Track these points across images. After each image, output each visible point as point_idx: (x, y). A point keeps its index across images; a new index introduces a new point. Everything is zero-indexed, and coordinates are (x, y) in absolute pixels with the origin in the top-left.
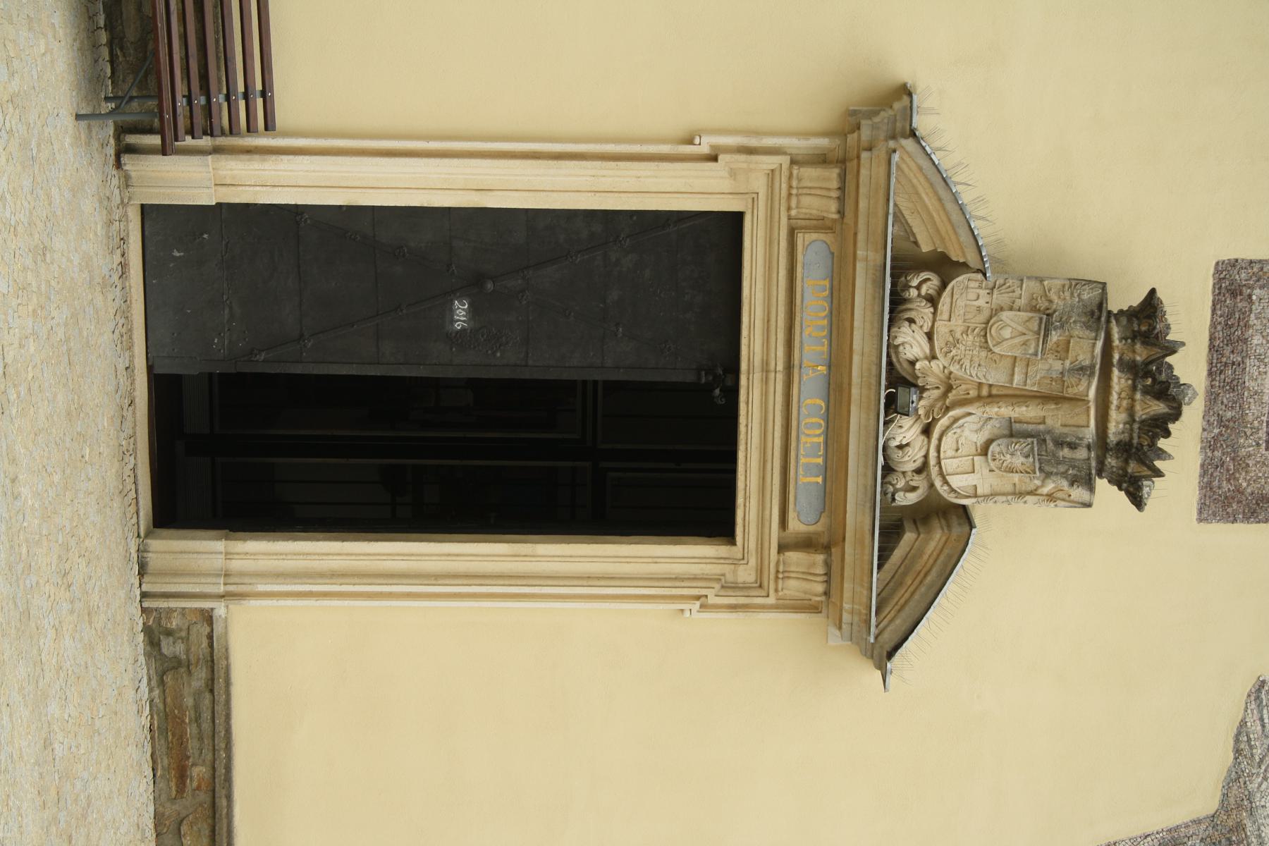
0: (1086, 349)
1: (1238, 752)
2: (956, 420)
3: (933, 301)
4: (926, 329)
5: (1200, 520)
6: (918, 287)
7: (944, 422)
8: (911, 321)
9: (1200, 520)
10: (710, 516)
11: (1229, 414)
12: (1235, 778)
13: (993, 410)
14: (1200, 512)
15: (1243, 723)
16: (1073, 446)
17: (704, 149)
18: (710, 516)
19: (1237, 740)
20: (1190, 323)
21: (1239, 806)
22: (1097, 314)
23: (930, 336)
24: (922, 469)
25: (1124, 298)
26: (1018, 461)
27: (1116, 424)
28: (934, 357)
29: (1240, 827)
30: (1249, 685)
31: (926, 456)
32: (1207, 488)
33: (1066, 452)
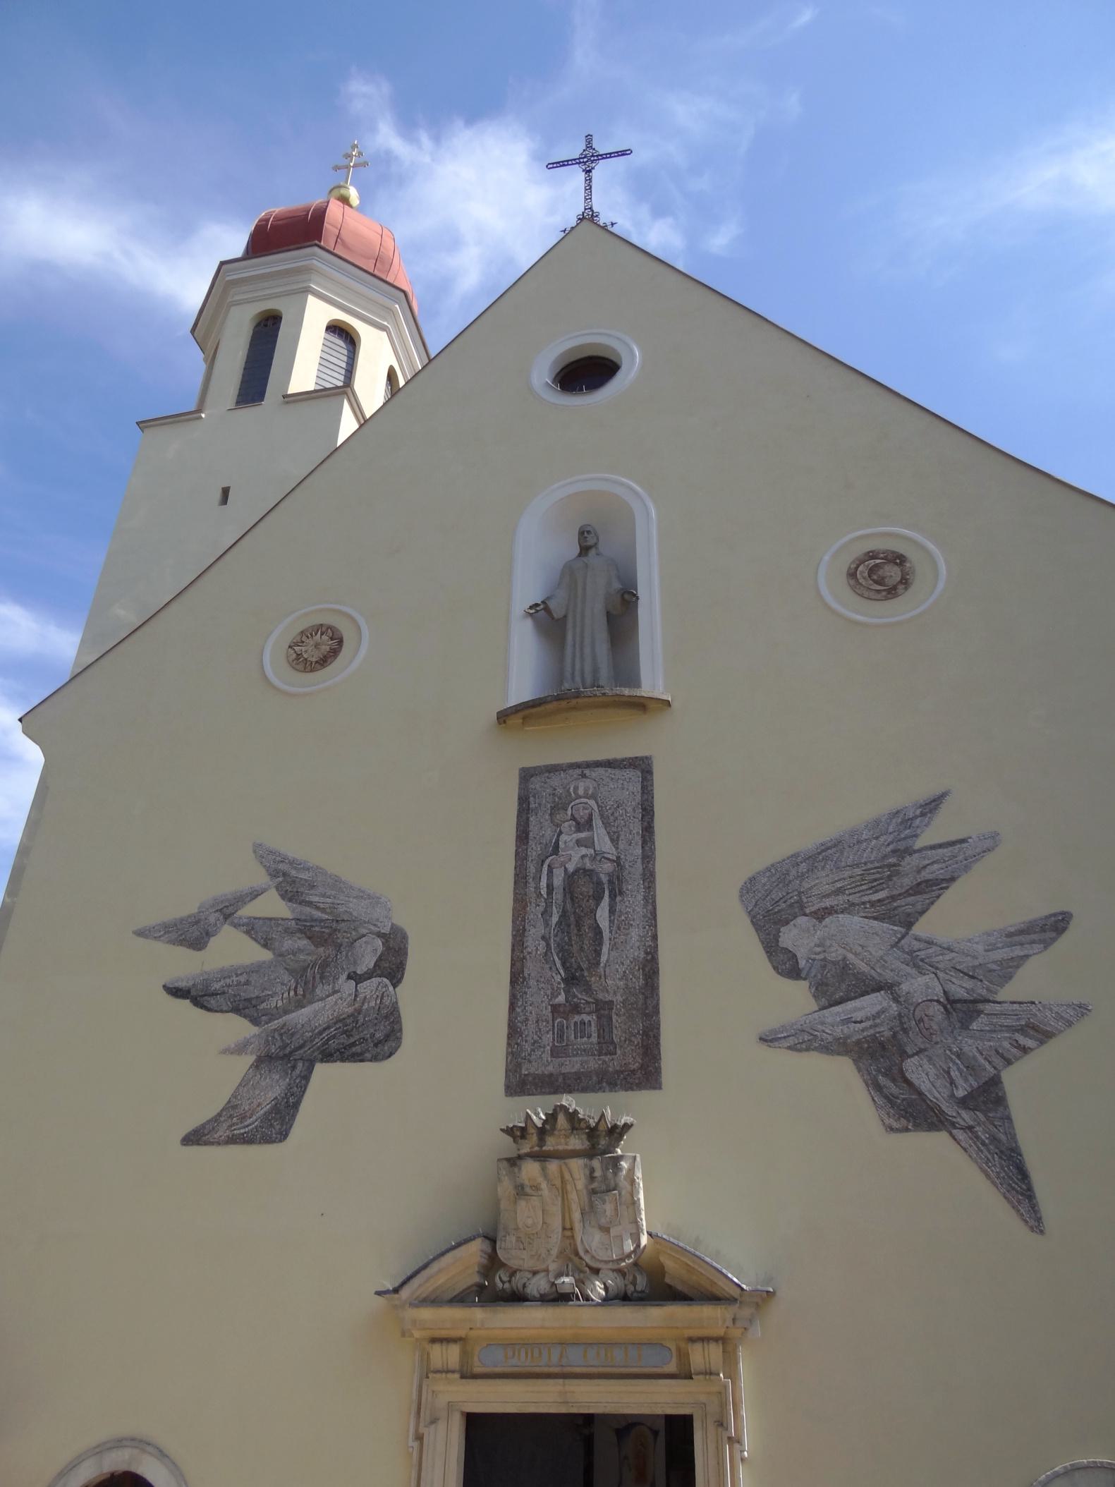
0: (530, 1169)
1: (808, 1049)
2: (587, 1252)
3: (513, 1273)
4: (530, 1276)
5: (660, 1088)
6: (503, 1282)
7: (587, 1259)
8: (524, 1286)
9: (660, 1088)
10: (678, 1430)
11: (594, 1078)
12: (826, 1049)
13: (578, 1226)
14: (655, 1088)
15: (789, 1048)
16: (592, 1170)
17: (416, 1444)
18: (678, 1430)
19: (800, 1051)
21: (845, 1044)
22: (514, 1162)
23: (535, 1273)
24: (621, 1272)
25: (507, 1146)
26: (609, 1208)
27: (577, 1143)
28: (547, 1271)
29: (858, 1042)
30: (764, 1047)
31: (613, 1270)
32: (639, 1086)
33: (598, 1173)
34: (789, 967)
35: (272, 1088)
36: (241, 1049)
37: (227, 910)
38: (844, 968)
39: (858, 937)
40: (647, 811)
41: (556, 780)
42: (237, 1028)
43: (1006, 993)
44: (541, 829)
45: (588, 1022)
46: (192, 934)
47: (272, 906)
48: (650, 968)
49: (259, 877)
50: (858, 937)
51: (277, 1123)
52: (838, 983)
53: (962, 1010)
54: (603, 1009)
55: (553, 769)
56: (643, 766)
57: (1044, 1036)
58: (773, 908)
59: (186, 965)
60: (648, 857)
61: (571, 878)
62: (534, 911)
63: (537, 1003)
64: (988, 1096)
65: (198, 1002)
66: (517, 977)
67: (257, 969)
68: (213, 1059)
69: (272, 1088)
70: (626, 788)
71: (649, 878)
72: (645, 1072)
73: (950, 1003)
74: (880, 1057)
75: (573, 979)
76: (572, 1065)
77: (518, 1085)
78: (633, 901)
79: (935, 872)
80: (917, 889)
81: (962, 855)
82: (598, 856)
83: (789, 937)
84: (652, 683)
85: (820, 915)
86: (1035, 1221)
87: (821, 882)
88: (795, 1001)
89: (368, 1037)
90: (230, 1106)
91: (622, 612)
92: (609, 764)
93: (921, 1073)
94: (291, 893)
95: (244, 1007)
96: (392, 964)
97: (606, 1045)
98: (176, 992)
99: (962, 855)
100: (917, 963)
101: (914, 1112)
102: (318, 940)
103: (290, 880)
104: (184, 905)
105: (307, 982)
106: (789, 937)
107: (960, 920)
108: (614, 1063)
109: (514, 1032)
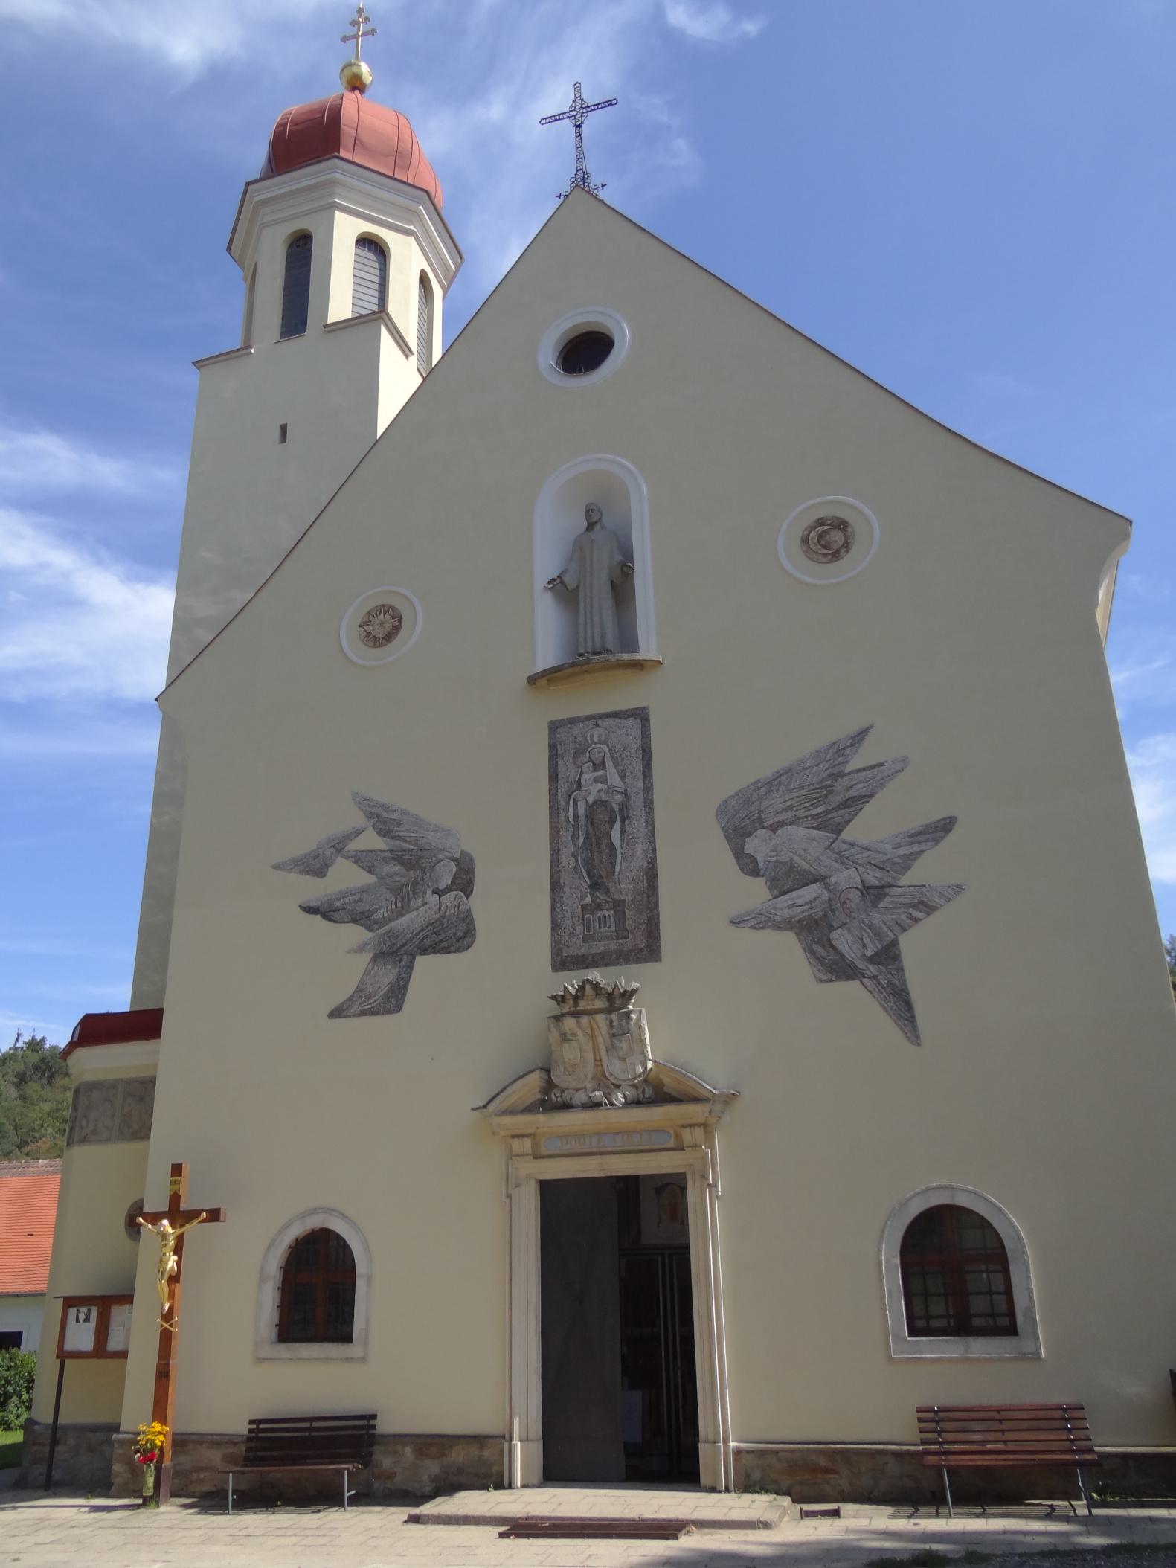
20: (571, 981)
34: (750, 867)
35: (387, 975)
36: (361, 948)
37: (338, 846)
38: (791, 866)
39: (801, 842)
40: (646, 752)
41: (576, 730)
42: (356, 934)
43: (904, 880)
44: (567, 770)
45: (609, 917)
46: (315, 866)
47: (371, 841)
48: (651, 874)
49: (357, 819)
50: (801, 842)
51: (394, 999)
52: (786, 878)
53: (873, 894)
54: (618, 906)
55: (573, 721)
56: (641, 715)
57: (929, 909)
58: (740, 825)
59: (315, 889)
60: (648, 789)
61: (591, 809)
62: (566, 835)
63: (572, 904)
64: (888, 955)
65: (326, 916)
66: (555, 886)
67: (366, 889)
68: (343, 956)
69: (387, 975)
70: (628, 734)
71: (649, 804)
72: (651, 951)
73: (866, 889)
74: (814, 931)
75: (595, 885)
76: (598, 947)
77: (561, 963)
78: (637, 824)
79: (860, 789)
80: (847, 803)
81: (880, 775)
82: (612, 790)
83: (751, 846)
84: (648, 648)
85: (774, 828)
86: (915, 1038)
87: (776, 802)
88: (756, 893)
89: (452, 936)
90: (359, 990)
91: (622, 586)
92: (616, 715)
93: (843, 941)
94: (384, 829)
95: (360, 918)
96: (464, 882)
97: (622, 932)
98: (310, 910)
99: (880, 775)
100: (843, 860)
101: (838, 969)
102: (409, 865)
103: (384, 822)
104: (306, 845)
105: (404, 897)
106: (751, 846)
107: (874, 826)
108: (628, 945)
109: (555, 926)
